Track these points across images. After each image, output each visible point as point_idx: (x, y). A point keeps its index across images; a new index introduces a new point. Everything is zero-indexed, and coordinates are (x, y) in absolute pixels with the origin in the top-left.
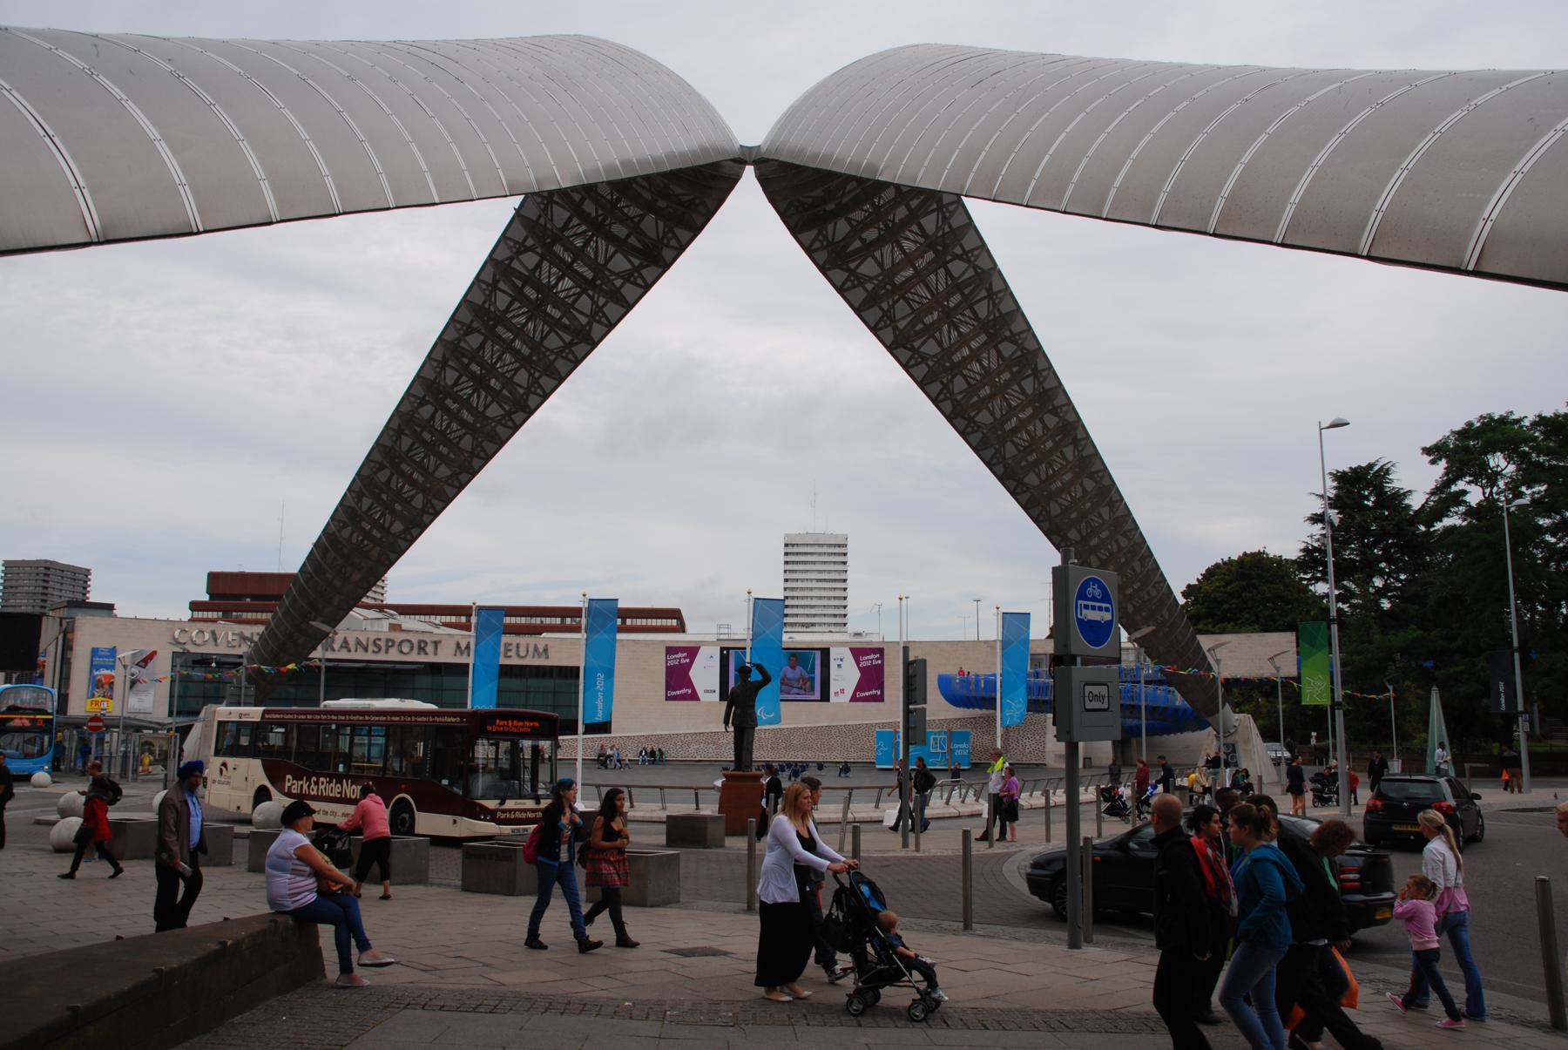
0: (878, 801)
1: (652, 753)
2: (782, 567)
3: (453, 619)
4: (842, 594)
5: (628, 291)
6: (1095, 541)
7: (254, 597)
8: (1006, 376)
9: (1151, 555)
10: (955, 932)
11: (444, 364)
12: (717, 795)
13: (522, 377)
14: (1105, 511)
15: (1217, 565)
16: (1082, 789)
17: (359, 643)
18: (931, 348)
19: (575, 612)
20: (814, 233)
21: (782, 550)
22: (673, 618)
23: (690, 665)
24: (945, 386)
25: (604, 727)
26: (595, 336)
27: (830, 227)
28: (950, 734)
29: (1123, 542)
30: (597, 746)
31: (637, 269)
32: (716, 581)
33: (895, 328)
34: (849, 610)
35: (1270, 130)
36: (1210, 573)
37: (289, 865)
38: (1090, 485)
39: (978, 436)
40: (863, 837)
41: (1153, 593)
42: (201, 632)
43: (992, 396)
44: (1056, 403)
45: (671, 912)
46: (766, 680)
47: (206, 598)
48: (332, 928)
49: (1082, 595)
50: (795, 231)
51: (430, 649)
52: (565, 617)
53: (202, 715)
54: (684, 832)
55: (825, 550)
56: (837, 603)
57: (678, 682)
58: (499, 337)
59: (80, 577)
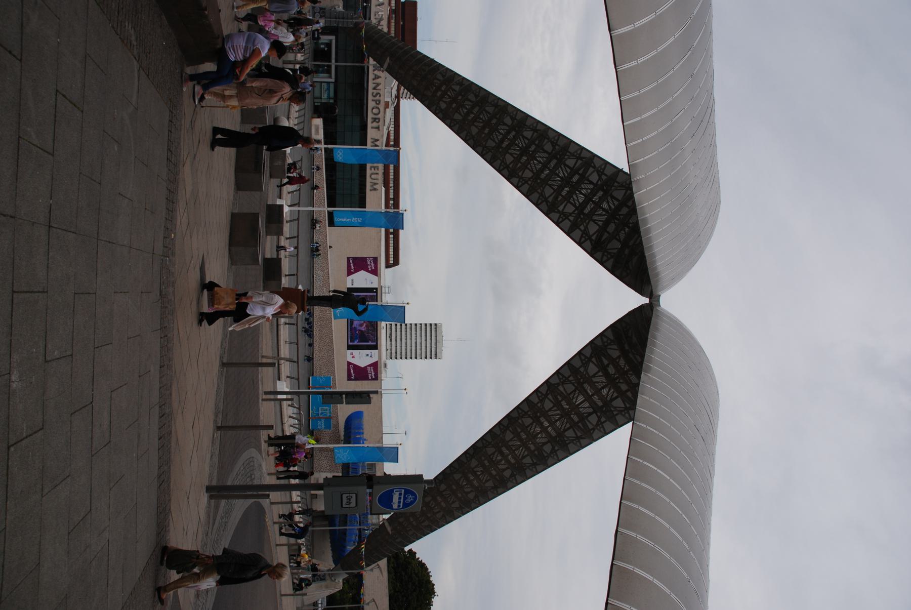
1: (317, 250)
2: (423, 322)
3: (392, 138)
6: (439, 499)
7: (403, 26)
8: (532, 447)
12: (293, 286)
13: (528, 174)
14: (457, 505)
16: (298, 493)
17: (378, 85)
18: (548, 405)
19: (396, 205)
20: (612, 338)
21: (433, 322)
23: (367, 270)
24: (526, 413)
25: (331, 223)
29: (439, 516)
31: (590, 238)
32: (417, 284)
33: (558, 384)
35: (673, 595)
36: (422, 566)
37: (250, 45)
39: (498, 432)
43: (521, 440)
45: (226, 259)
51: (375, 124)
52: (394, 200)
55: (433, 346)
56: (404, 353)
57: (358, 264)
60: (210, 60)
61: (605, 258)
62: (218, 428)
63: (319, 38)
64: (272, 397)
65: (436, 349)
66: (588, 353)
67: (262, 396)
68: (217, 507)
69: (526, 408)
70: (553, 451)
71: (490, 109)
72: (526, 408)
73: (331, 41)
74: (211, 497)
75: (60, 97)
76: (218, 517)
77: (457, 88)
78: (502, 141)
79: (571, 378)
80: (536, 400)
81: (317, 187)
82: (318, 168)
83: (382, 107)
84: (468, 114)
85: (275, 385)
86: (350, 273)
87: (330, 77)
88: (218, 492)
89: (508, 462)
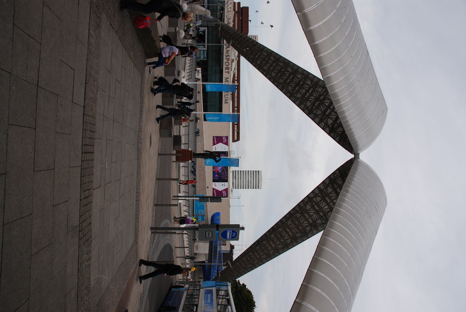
0: (185, 192)
1: (198, 132)
2: (252, 170)
3: (236, 76)
4: (244, 187)
6: (256, 254)
7: (242, 20)
8: (301, 228)
9: (252, 270)
10: (154, 202)
11: (303, 74)
12: (187, 149)
13: (299, 95)
14: (264, 257)
15: (251, 294)
16: (189, 260)
17: (228, 51)
18: (308, 207)
19: (238, 111)
20: (338, 174)
21: (257, 170)
22: (237, 138)
23: (223, 143)
24: (298, 211)
25: (205, 120)
26: (310, 115)
27: (340, 179)
28: (204, 215)
29: (256, 262)
30: (200, 117)
31: (328, 126)
32: (248, 152)
33: (313, 197)
34: (240, 189)
35: (338, 270)
36: (249, 292)
37: (171, 51)
38: (271, 252)
39: (284, 221)
40: (176, 181)
41: (242, 270)
42: (231, 8)
43: (295, 224)
44: (294, 243)
45: (159, 135)
46: (217, 161)
47: (241, 6)
49: (233, 231)
50: (339, 169)
51: (227, 70)
52: (237, 108)
53: (207, 10)
54: (177, 140)
55: (257, 182)
56: (242, 186)
57: (218, 140)
58: (310, 89)
60: (156, 57)
61: (335, 136)
62: (155, 205)
63: (199, 29)
64: (176, 198)
66: (327, 182)
67: (172, 198)
68: (154, 238)
69: (298, 209)
70: (311, 230)
71: (281, 64)
72: (298, 209)
73: (205, 30)
74: (152, 233)
75: (40, 42)
76: (154, 243)
77: (265, 54)
78: (287, 79)
79: (319, 194)
80: (302, 205)
81: (198, 102)
82: (199, 92)
83: (230, 62)
84: (270, 66)
85: (178, 194)
86: (214, 144)
87: (205, 48)
88: (155, 230)
89: (289, 235)
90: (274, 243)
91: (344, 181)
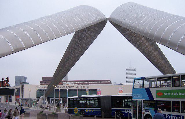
5: (94, 38)
18: (138, 43)
48: (152, 82)
59: (25, 78)
65: (23, 91)
83: (68, 86)
90: (79, 44)
91: (127, 30)
